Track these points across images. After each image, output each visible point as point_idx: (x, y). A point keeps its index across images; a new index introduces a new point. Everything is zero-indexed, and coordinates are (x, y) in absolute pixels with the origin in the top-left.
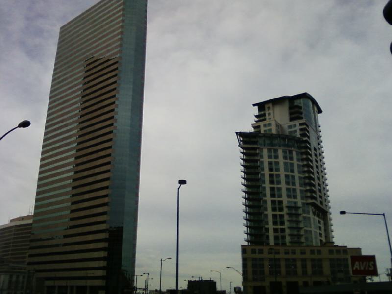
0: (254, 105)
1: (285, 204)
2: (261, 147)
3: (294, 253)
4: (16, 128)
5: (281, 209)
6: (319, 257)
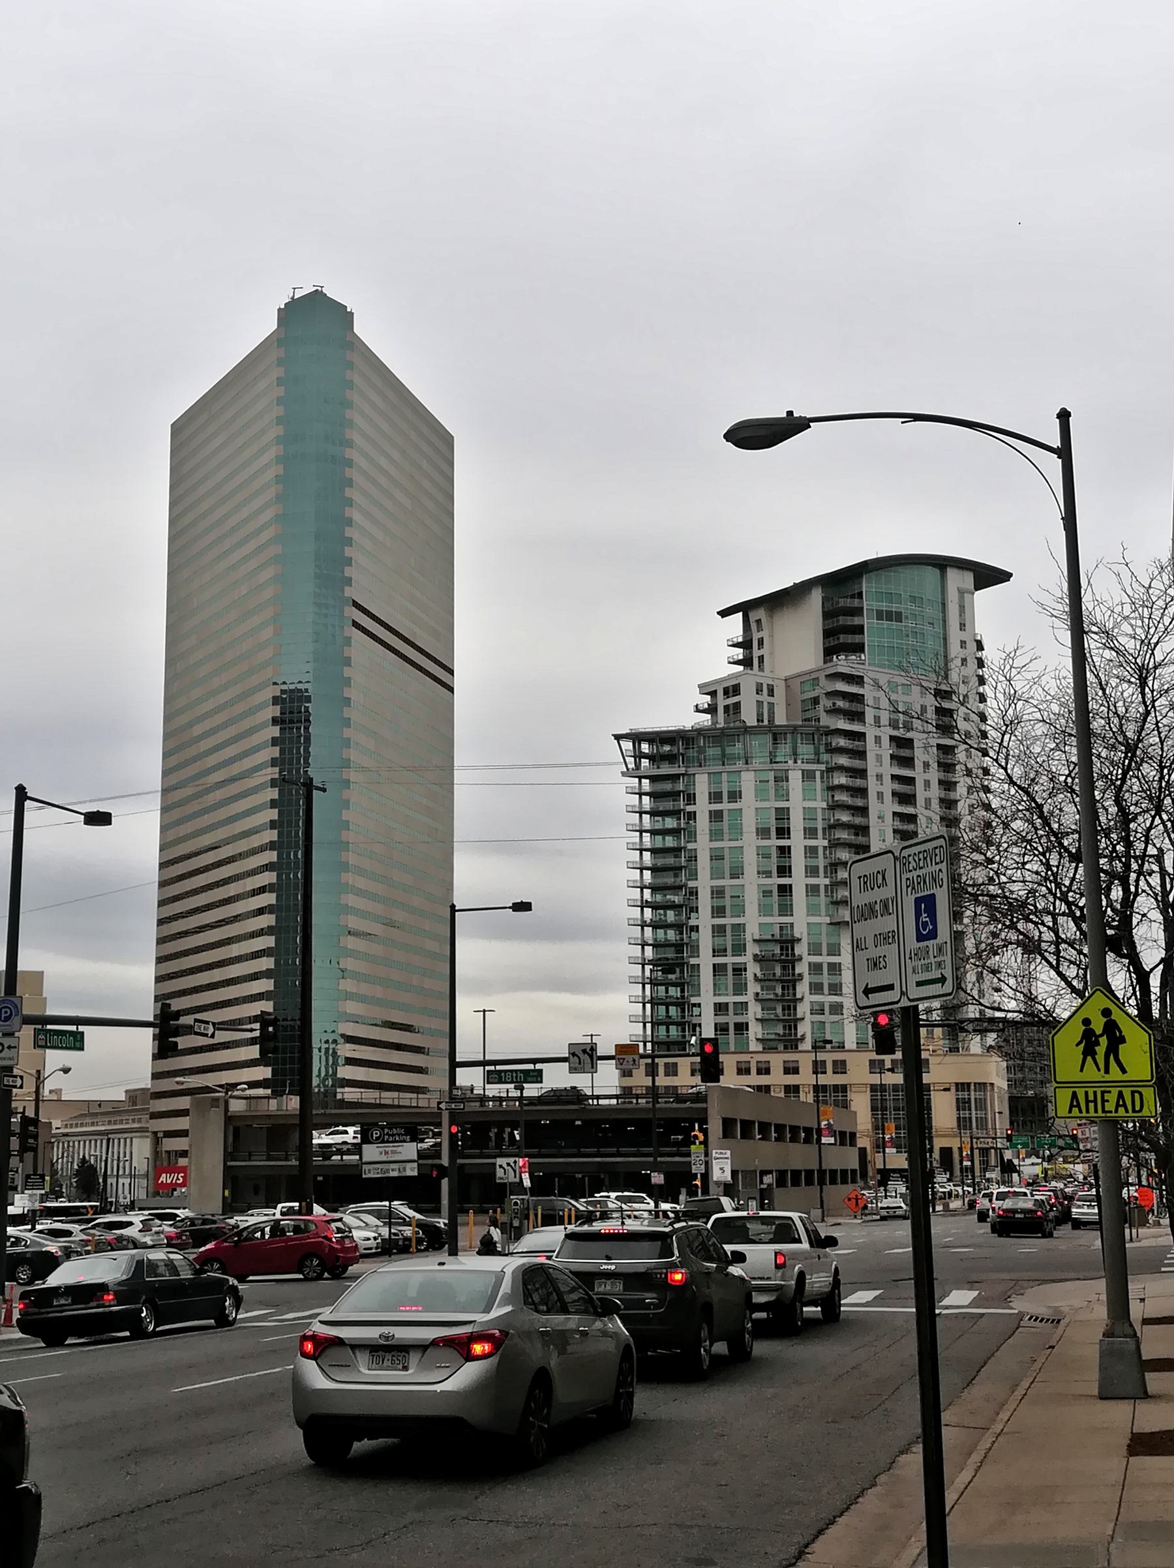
0: (724, 613)
1: (752, 931)
2: (691, 771)
3: (764, 1070)
4: (821, 1197)
5: (739, 949)
6: (839, 1080)
